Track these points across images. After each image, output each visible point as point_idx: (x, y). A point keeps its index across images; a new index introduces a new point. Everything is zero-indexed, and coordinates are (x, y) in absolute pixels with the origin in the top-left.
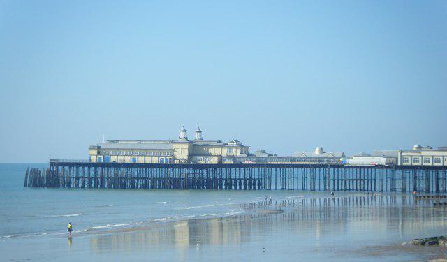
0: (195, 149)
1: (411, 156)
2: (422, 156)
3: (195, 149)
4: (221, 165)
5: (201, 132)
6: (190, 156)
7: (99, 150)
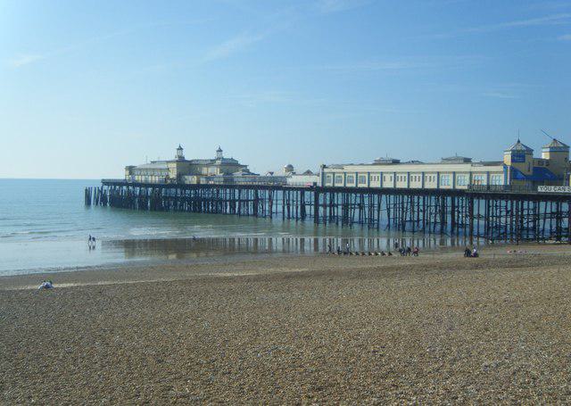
0: (131, 169)
1: (334, 173)
2: (345, 173)
3: (186, 166)
4: (198, 186)
5: (181, 149)
6: (179, 176)
7: (131, 169)
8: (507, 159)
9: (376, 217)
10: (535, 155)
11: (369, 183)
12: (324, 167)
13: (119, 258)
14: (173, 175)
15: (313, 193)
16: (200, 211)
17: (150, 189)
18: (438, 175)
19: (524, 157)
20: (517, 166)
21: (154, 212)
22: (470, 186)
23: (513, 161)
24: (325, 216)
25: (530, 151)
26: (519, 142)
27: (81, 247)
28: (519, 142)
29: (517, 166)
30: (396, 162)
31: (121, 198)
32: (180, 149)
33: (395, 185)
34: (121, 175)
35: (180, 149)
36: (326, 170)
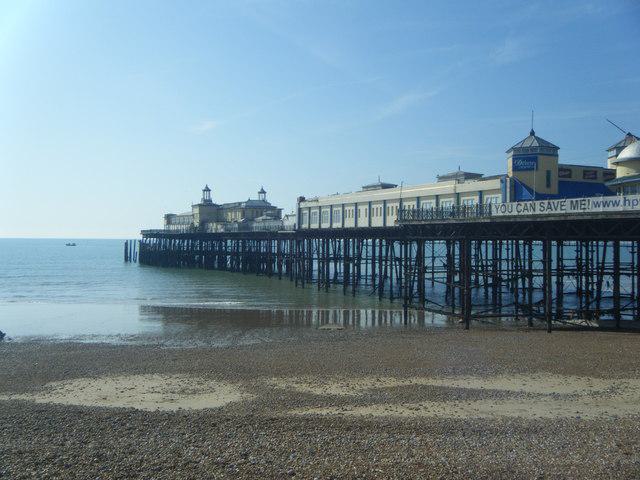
0: (169, 218)
3: (210, 210)
6: (203, 223)
7: (169, 218)
8: (506, 167)
9: (389, 275)
10: (565, 158)
11: (331, 224)
12: (302, 199)
13: (156, 326)
14: (197, 224)
15: (622, 243)
16: (213, 268)
17: (437, 252)
18: (370, 206)
19: (535, 159)
20: (523, 177)
21: (253, 277)
22: (400, 219)
23: (515, 168)
24: (524, 288)
25: (551, 150)
26: (532, 133)
27: (119, 311)
28: (532, 133)
29: (523, 177)
30: (385, 186)
31: (161, 253)
32: (207, 190)
33: (370, 222)
34: (160, 225)
35: (207, 190)
36: (303, 205)
